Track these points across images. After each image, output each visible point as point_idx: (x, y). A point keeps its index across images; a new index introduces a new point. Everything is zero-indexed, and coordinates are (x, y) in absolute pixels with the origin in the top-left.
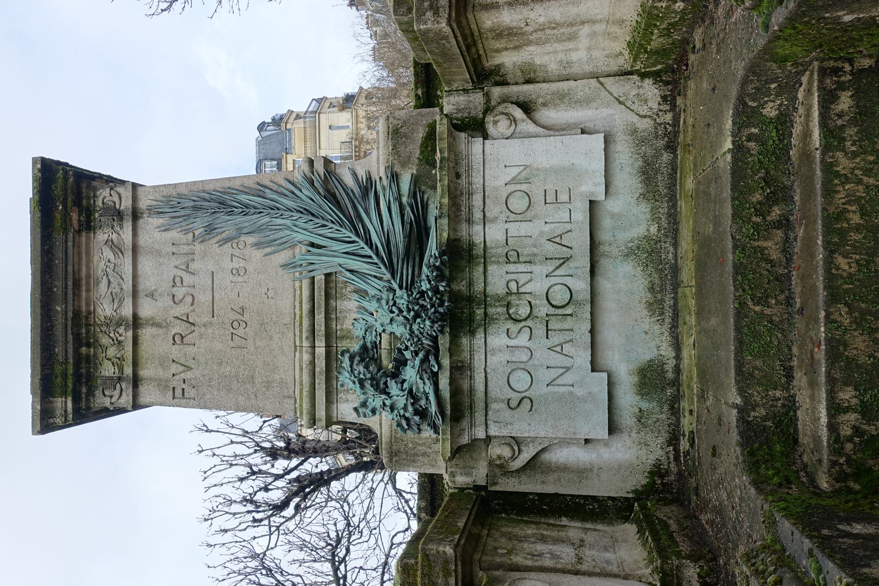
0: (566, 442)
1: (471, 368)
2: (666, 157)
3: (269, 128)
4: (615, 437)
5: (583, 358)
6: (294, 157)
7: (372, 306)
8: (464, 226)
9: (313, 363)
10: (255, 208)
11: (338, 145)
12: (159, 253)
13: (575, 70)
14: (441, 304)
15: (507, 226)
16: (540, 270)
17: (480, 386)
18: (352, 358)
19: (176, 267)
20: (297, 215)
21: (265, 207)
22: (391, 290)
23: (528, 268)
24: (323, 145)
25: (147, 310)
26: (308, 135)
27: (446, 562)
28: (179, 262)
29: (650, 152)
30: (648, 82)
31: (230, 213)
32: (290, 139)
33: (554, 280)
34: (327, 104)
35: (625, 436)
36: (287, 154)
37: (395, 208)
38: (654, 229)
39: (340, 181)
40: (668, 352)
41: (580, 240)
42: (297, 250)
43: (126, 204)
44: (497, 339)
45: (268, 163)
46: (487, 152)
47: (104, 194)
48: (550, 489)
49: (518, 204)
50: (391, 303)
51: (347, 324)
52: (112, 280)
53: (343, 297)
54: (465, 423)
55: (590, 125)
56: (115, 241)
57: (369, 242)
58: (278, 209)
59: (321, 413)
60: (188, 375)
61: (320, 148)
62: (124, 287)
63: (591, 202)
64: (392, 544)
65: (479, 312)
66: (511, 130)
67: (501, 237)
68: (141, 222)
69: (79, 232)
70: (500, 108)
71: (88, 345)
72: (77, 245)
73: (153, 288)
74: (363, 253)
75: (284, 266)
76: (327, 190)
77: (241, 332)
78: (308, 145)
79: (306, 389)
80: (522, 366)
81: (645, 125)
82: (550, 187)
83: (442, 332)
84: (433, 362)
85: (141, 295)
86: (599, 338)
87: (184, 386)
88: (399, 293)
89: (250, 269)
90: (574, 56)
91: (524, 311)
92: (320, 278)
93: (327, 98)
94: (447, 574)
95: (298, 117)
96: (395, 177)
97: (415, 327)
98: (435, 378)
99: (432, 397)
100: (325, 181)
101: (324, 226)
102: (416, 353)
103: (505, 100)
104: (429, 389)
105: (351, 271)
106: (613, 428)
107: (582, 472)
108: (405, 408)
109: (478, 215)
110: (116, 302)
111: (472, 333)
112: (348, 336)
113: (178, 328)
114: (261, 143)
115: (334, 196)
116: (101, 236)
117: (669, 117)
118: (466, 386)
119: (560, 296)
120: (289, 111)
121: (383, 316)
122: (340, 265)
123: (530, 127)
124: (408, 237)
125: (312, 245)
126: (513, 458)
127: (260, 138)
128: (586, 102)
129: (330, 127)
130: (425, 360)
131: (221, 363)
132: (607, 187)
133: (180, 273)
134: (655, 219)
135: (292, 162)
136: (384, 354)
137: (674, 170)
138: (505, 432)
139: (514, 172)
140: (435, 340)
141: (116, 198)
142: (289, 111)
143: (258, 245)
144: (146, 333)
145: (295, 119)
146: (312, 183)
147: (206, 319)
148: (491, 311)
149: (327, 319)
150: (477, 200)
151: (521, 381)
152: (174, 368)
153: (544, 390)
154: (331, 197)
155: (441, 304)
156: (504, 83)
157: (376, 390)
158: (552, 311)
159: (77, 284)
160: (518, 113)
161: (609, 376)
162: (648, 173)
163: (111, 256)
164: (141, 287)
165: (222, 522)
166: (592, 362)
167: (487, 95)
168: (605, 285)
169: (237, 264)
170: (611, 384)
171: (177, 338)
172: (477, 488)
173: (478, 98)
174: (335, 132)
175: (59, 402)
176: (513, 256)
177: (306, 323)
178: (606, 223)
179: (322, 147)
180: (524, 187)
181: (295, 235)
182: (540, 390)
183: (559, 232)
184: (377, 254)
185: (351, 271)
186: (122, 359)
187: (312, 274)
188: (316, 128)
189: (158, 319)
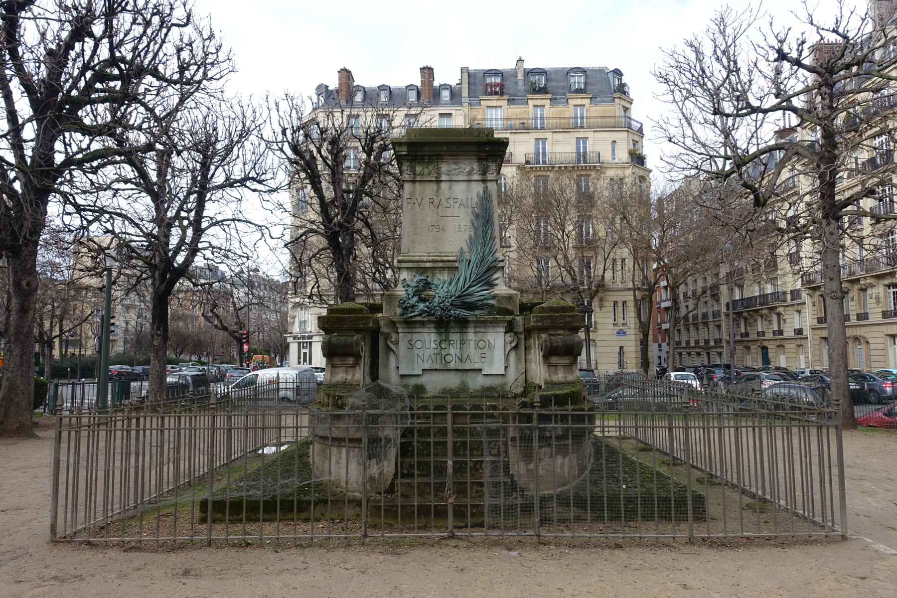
0: (397, 360)
1: (423, 327)
2: (496, 395)
3: (617, 80)
5: (427, 366)
6: (587, 106)
7: (445, 288)
8: (474, 325)
9: (423, 261)
11: (597, 149)
12: (468, 192)
13: (528, 364)
16: (458, 352)
17: (416, 331)
18: (425, 280)
20: (481, 255)
21: (486, 241)
22: (451, 297)
23: (458, 348)
24: (598, 135)
25: (444, 186)
26: (608, 120)
27: (367, 324)
29: (498, 390)
30: (523, 389)
31: (483, 224)
32: (604, 102)
33: (454, 356)
34: (636, 138)
35: (399, 380)
36: (591, 98)
37: (482, 298)
38: (471, 391)
39: (495, 273)
40: (429, 395)
41: (468, 366)
42: (467, 254)
43: (490, 177)
44: (433, 337)
45: (582, 80)
47: (493, 167)
48: (380, 354)
49: (481, 344)
51: (438, 276)
53: (449, 274)
54: (403, 325)
55: (508, 369)
57: (470, 287)
59: (403, 265)
60: (417, 206)
61: (594, 131)
64: (261, 227)
65: (443, 330)
67: (470, 338)
68: (481, 183)
69: (477, 156)
70: (516, 338)
71: (429, 159)
72: (471, 155)
75: (461, 249)
76: (491, 267)
77: (435, 229)
78: (599, 120)
79: (411, 258)
81: (508, 388)
83: (436, 318)
85: (450, 183)
86: (434, 372)
88: (450, 300)
89: (461, 233)
90: (533, 364)
91: (443, 346)
92: (456, 265)
93: (643, 137)
94: (363, 324)
95: (626, 109)
96: (494, 297)
97: (438, 308)
98: (420, 315)
99: (413, 314)
100: (495, 267)
102: (428, 308)
103: (519, 339)
104: (416, 313)
105: (459, 279)
106: (402, 376)
107: (386, 365)
108: (408, 303)
109: (478, 330)
111: (435, 328)
112: (434, 275)
113: (436, 201)
114: (601, 72)
115: (489, 270)
116: (475, 166)
117: (510, 396)
118: (417, 325)
119: (448, 358)
120: (632, 100)
121: (442, 294)
123: (508, 349)
124: (471, 303)
125: (470, 261)
126: (391, 342)
127: (606, 71)
128: (517, 368)
129: (614, 142)
130: (426, 311)
133: (459, 201)
134: (475, 391)
135: (582, 103)
136: (427, 293)
137: (492, 397)
138: (400, 339)
139: (492, 342)
140: (433, 315)
141: (491, 172)
142: (632, 100)
143: (470, 237)
144: (434, 186)
145: (624, 107)
146: (495, 261)
147: (440, 214)
148: (443, 334)
149: (440, 267)
150: (483, 330)
151: (419, 345)
152: (419, 199)
153: (416, 353)
154: (489, 269)
156: (525, 340)
159: (456, 155)
160: (514, 344)
162: (491, 389)
163: (467, 170)
164: (453, 183)
165: (284, 106)
167: (521, 333)
168: (452, 374)
169: (463, 227)
170: (418, 376)
171: (432, 200)
172: (379, 328)
173: (521, 329)
174: (609, 147)
175: (405, 148)
177: (439, 258)
178: (474, 375)
179: (596, 133)
180: (487, 346)
182: (416, 351)
184: (465, 291)
185: (459, 279)
186: (423, 175)
188: (614, 127)
189: (440, 192)
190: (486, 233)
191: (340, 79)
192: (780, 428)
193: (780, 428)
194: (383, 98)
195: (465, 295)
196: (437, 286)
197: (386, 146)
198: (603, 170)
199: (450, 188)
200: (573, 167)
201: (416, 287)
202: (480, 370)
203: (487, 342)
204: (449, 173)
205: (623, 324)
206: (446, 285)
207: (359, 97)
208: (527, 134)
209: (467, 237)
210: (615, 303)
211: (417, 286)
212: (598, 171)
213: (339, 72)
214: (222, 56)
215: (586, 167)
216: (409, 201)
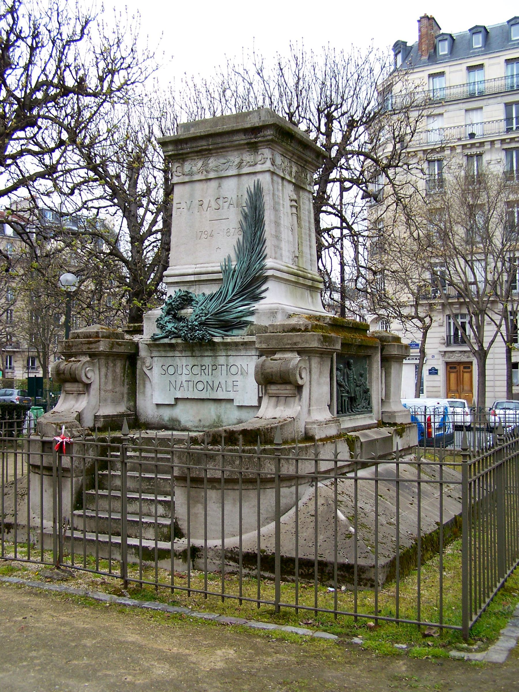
4: (155, 406)
23: (210, 373)
27: (98, 348)
33: (205, 384)
35: (156, 410)
41: (220, 395)
57: (230, 301)
75: (229, 257)
86: (187, 401)
102: (176, 328)
110: (216, 169)
125: (235, 271)
132: (242, 406)
139: (245, 368)
155: (191, 339)
163: (236, 163)
169: (232, 231)
176: (214, 367)
180: (239, 373)
191: (420, 31)
192: (21, 455)
193: (21, 455)
194: (478, 41)
195: (222, 312)
199: (220, 186)
202: (232, 400)
203: (239, 367)
207: (443, 49)
213: (419, 21)
214: (139, 55)
216: (179, 206)
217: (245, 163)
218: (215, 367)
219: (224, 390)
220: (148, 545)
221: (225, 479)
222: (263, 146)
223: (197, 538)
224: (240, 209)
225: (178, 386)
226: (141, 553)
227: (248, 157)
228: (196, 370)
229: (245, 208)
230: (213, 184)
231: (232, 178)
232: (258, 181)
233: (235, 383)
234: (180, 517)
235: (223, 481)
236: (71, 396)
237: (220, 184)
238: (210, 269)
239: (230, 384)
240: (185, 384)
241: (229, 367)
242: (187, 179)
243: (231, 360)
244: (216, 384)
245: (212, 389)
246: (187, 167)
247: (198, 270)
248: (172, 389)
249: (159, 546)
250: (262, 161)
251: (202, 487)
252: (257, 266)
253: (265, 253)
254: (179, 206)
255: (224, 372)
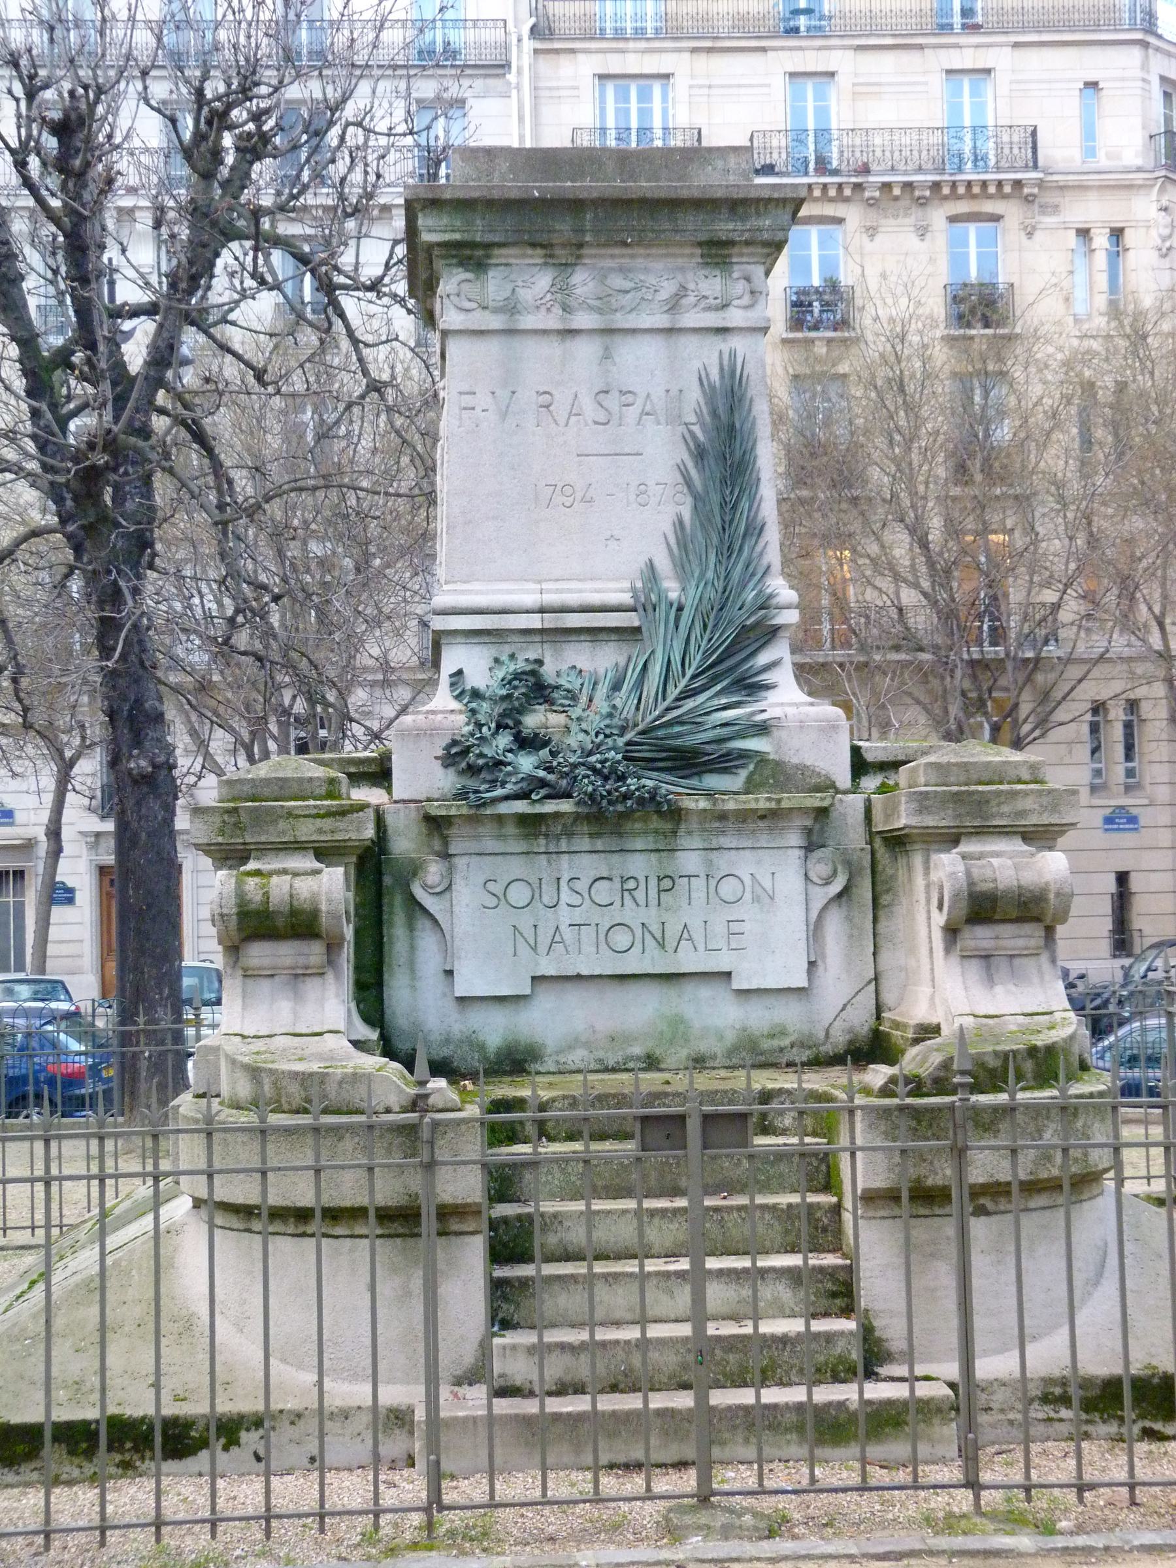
10: (731, 522)
14: (610, 803)
15: (703, 875)
19: (648, 396)
20: (720, 585)
28: (655, 401)
33: (638, 932)
35: (455, 1015)
41: (688, 961)
46: (790, 851)
50: (608, 731)
52: (629, 296)
56: (684, 301)
58: (729, 557)
61: (1016, 45)
62: (618, 315)
63: (729, 974)
66: (815, 879)
73: (617, 360)
74: (670, 687)
75: (651, 565)
80: (537, 895)
82: (746, 927)
84: (543, 792)
85: (607, 339)
86: (568, 986)
87: (478, 410)
98: (524, 795)
101: (705, 626)
102: (550, 770)
104: (509, 788)
108: (481, 755)
110: (597, 303)
122: (653, 652)
123: (816, 906)
125: (680, 609)
126: (425, 887)
129: (1093, 85)
130: (543, 783)
131: (513, 468)
132: (748, 991)
133: (639, 402)
139: (767, 884)
143: (680, 523)
157: (500, 715)
158: (603, 930)
161: (525, 997)
163: (664, 295)
164: (618, 339)
166: (543, 978)
176: (667, 883)
178: (705, 992)
180: (748, 896)
181: (694, 583)
183: (694, 936)
187: (640, 610)
190: (734, 508)
195: (669, 724)
196: (573, 696)
197: (265, 138)
198: (1049, 198)
200: (936, 186)
201: (504, 698)
203: (747, 880)
204: (603, 305)
205: (1128, 788)
206: (602, 690)
208: (759, 55)
209: (667, 526)
210: (1098, 708)
211: (508, 697)
212: (1029, 200)
215: (984, 184)
216: (467, 400)
217: (691, 299)
218: (667, 882)
219: (701, 947)
220: (842, 1397)
221: (1022, 1183)
222: (752, 254)
223: (938, 1360)
224: (682, 429)
225: (544, 939)
226: (809, 1426)
227: (710, 285)
228: (603, 892)
229: (697, 429)
230: (586, 351)
231: (647, 338)
232: (733, 355)
233: (735, 927)
234: (878, 1306)
235: (1015, 1189)
236: (266, 984)
237: (607, 349)
238: (596, 599)
239: (719, 928)
240: (568, 934)
241: (713, 882)
242: (495, 322)
243: (723, 862)
244: (673, 931)
245: (662, 945)
246: (495, 284)
247: (551, 599)
248: (524, 950)
249: (600, 1407)
250: (746, 300)
251: (947, 1210)
252: (750, 596)
253: (765, 562)
254: (467, 400)
255: (699, 895)
